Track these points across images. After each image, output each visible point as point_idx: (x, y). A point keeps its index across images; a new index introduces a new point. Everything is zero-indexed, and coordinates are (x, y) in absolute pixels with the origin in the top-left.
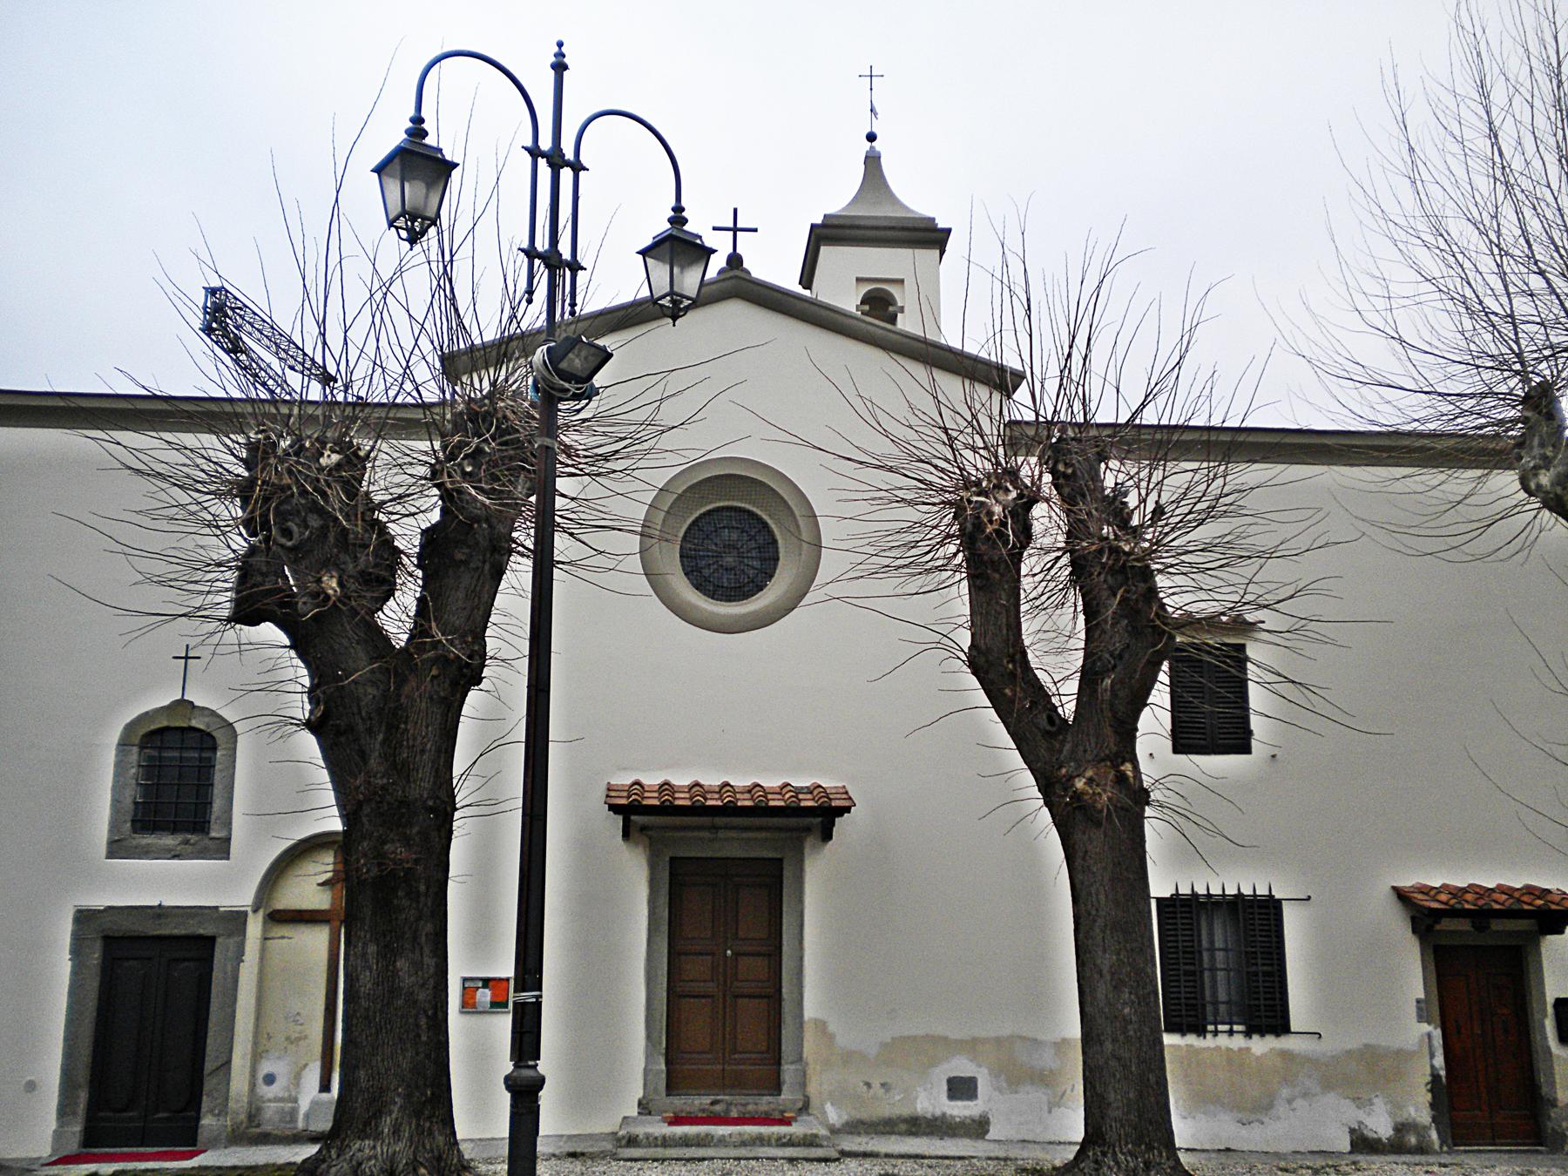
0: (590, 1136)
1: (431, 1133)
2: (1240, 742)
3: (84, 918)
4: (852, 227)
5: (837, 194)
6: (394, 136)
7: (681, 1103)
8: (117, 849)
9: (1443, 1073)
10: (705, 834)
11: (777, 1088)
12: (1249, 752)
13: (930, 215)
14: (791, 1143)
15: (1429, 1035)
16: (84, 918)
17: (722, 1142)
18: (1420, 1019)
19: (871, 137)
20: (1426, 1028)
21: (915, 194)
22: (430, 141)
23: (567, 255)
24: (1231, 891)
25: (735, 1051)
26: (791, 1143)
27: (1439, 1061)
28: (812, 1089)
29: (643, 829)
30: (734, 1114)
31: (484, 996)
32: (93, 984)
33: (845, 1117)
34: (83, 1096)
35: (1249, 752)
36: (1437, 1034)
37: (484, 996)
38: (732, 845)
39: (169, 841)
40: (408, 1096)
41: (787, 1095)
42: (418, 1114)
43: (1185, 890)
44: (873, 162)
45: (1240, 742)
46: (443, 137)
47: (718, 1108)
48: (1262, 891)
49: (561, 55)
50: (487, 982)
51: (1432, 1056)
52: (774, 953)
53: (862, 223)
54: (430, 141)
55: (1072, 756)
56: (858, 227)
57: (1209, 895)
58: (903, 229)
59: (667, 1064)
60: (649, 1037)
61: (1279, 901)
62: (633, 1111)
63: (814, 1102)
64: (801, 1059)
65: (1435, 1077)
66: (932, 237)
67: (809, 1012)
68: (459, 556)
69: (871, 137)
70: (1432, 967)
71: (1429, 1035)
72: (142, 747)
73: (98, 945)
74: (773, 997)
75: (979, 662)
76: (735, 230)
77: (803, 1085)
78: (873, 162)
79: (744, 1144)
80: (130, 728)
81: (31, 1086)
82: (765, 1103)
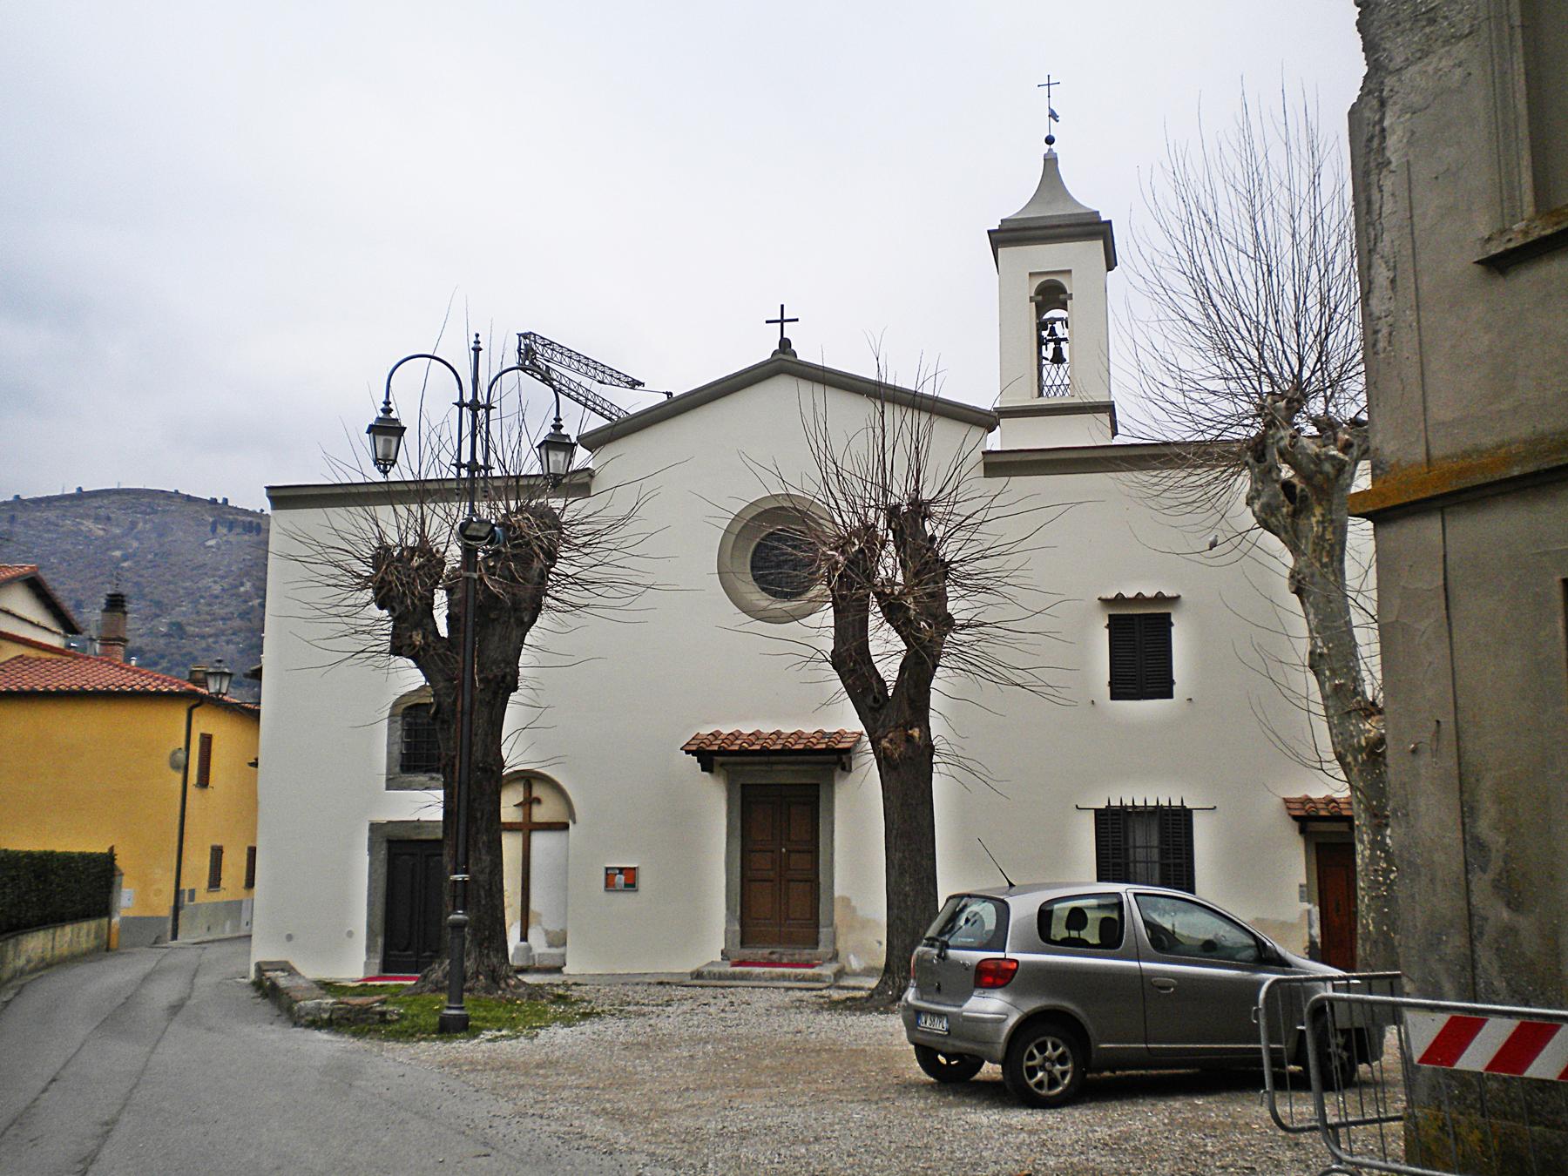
0: (672, 974)
1: (488, 956)
2: (1164, 689)
3: (375, 828)
4: (1025, 229)
5: (1015, 196)
6: (373, 415)
7: (748, 953)
8: (391, 784)
9: (1318, 940)
10: (764, 768)
11: (816, 944)
12: (1171, 696)
13: (1095, 209)
14: (804, 979)
15: (1309, 912)
16: (375, 828)
17: (758, 977)
18: (1302, 899)
19: (1050, 140)
20: (1307, 906)
21: (1087, 191)
22: (393, 415)
23: (481, 462)
24: (1152, 803)
25: (788, 918)
26: (804, 979)
27: (1316, 931)
28: (840, 945)
29: (722, 765)
30: (785, 961)
31: (620, 879)
32: (382, 870)
33: (863, 966)
34: (380, 941)
35: (1171, 696)
36: (1316, 910)
37: (620, 879)
38: (785, 776)
39: (422, 778)
40: (474, 935)
41: (821, 949)
42: (480, 945)
43: (1115, 803)
44: (1051, 162)
45: (1164, 689)
46: (404, 413)
47: (774, 957)
48: (1176, 803)
49: (477, 342)
50: (621, 870)
51: (1310, 926)
52: (814, 851)
53: (1032, 224)
54: (393, 415)
55: (883, 725)
56: (1030, 229)
57: (1134, 806)
58: (1079, 225)
59: (741, 926)
60: (728, 908)
61: (1190, 811)
62: (719, 958)
63: (842, 955)
64: (832, 924)
65: (1312, 943)
66: (1096, 229)
67: (838, 891)
68: (492, 616)
69: (1050, 140)
70: (1314, 861)
71: (1309, 912)
72: (404, 716)
73: (384, 845)
74: (814, 882)
75: (837, 661)
76: (782, 321)
77: (834, 941)
78: (1051, 162)
79: (772, 979)
80: (395, 705)
81: (350, 934)
82: (806, 954)
